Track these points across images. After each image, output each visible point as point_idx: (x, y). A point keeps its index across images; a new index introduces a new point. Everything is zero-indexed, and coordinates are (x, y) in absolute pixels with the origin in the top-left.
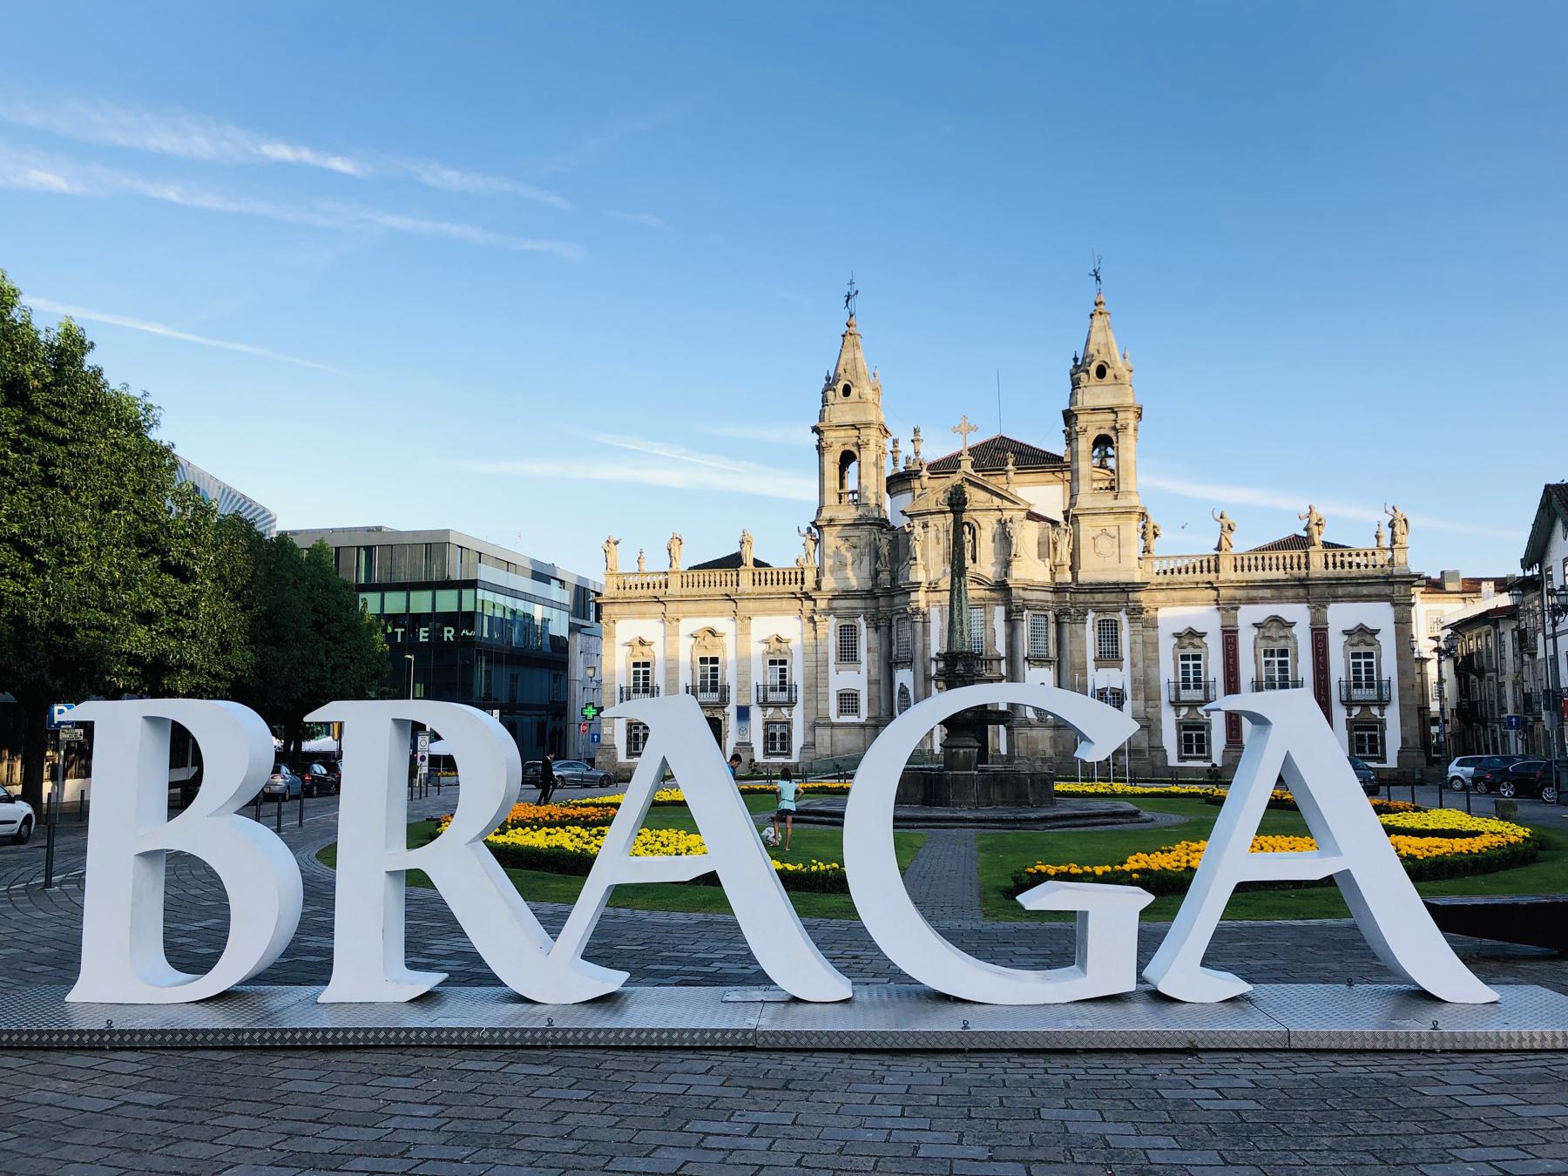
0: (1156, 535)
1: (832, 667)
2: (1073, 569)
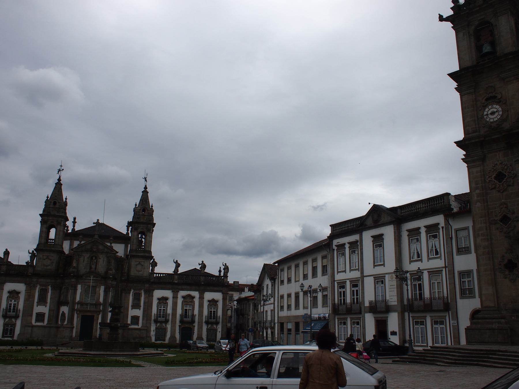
1: (35, 304)
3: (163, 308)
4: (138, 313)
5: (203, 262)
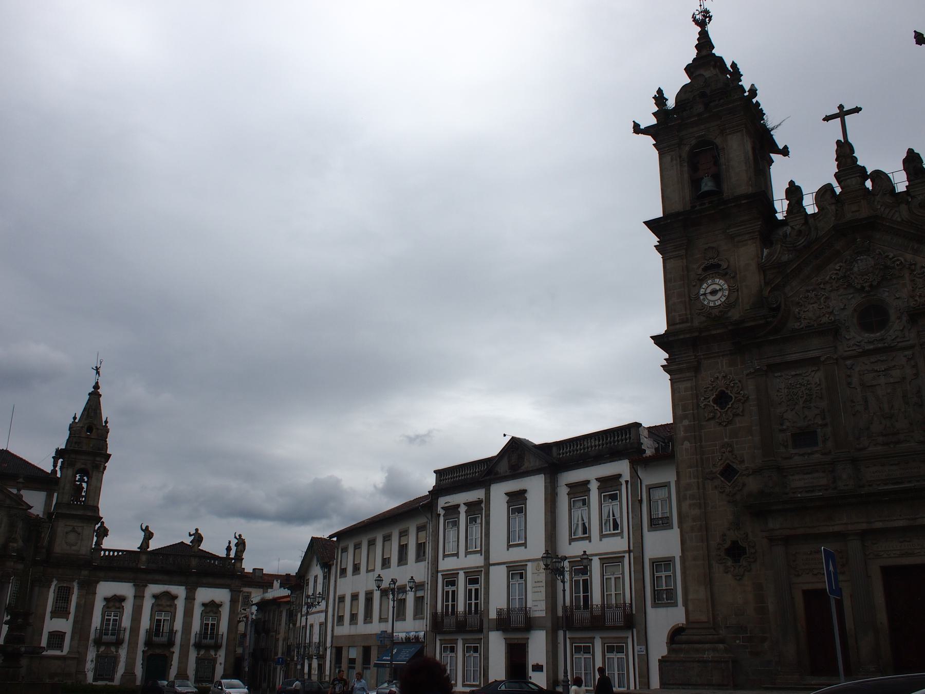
3: (114, 616)
4: (64, 625)
5: (197, 530)
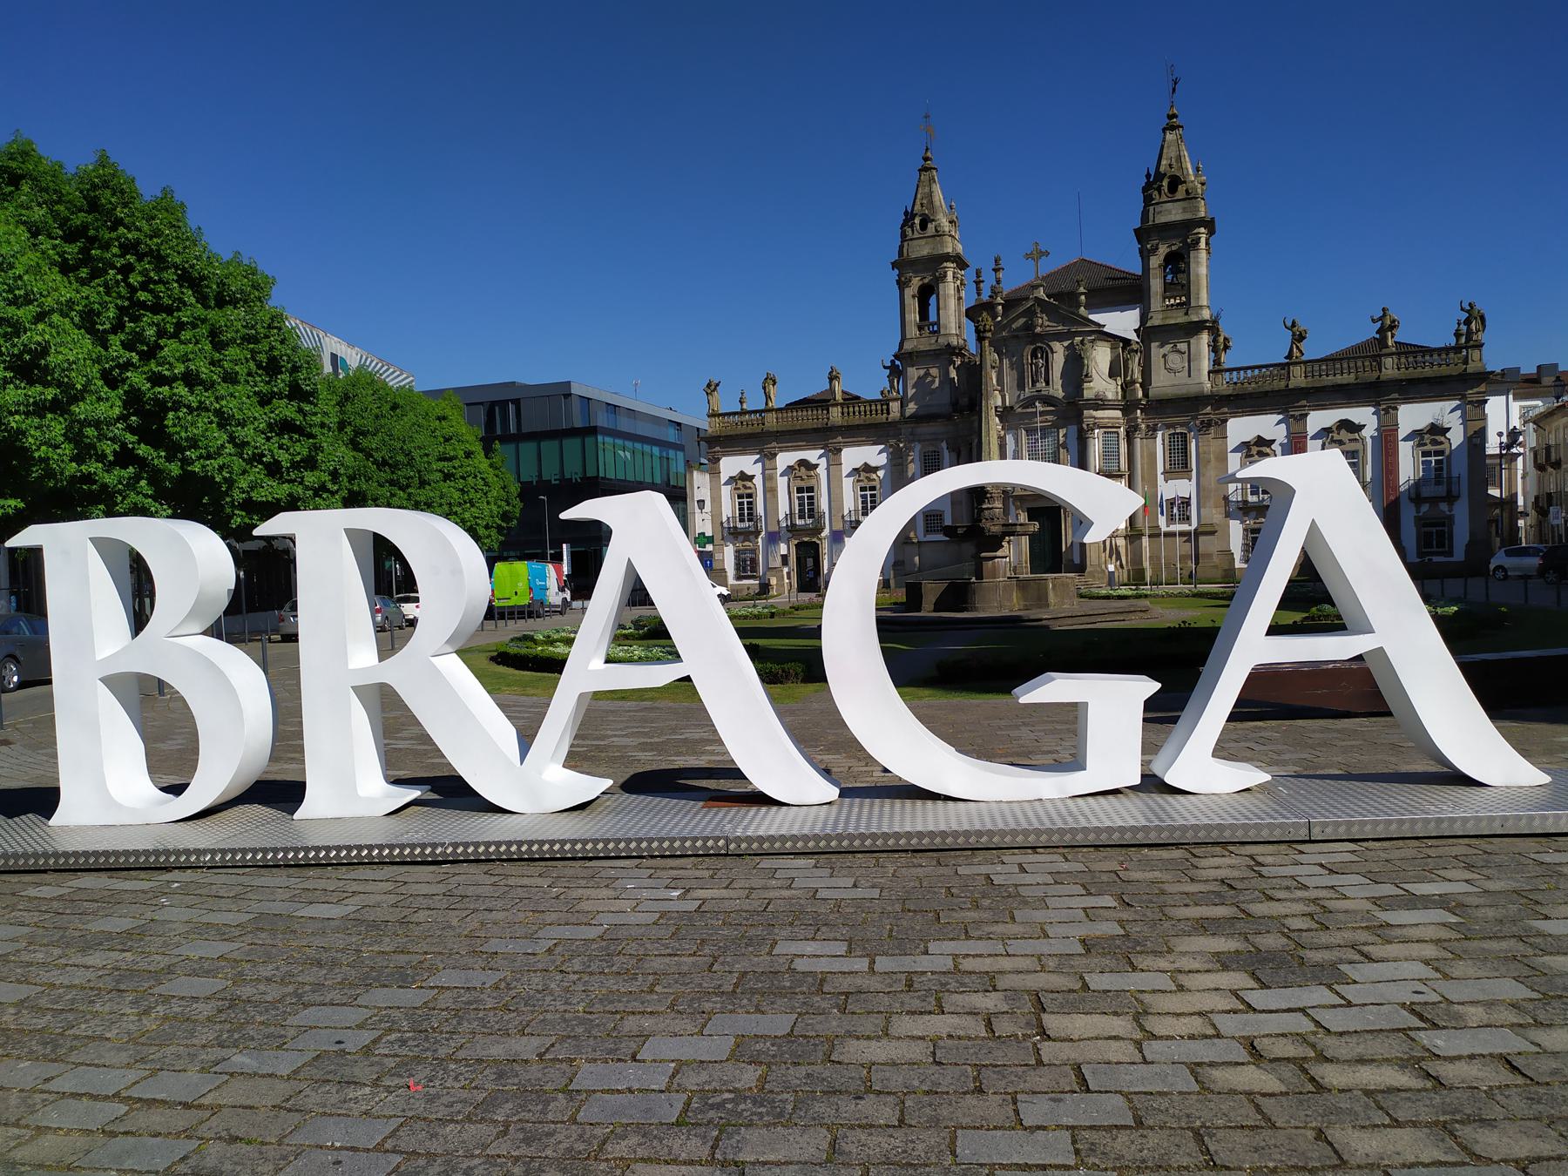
0: (1226, 348)
2: (1145, 385)
